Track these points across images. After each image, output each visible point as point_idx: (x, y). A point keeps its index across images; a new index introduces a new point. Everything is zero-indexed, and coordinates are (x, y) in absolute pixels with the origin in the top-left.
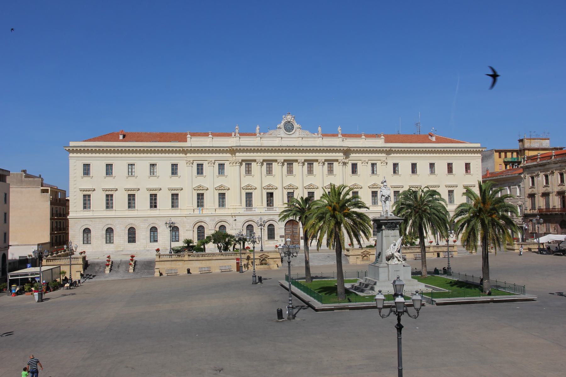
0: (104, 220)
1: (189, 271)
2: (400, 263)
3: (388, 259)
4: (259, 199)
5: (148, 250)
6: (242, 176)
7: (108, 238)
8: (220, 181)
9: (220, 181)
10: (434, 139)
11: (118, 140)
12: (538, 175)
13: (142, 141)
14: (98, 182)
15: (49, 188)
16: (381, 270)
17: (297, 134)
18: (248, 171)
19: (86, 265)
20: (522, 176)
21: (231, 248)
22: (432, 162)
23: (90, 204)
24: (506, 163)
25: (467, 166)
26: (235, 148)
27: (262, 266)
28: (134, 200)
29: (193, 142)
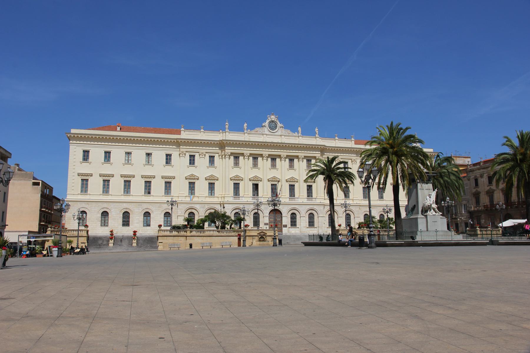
0: (100, 204)
1: (191, 246)
4: (246, 189)
8: (211, 172)
14: (96, 166)
15: (41, 182)
17: (279, 133)
21: (228, 227)
27: (261, 243)
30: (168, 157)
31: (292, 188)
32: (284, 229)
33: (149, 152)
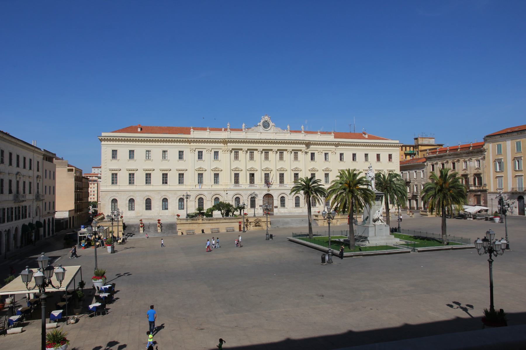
0: (127, 193)
1: (203, 231)
2: (383, 224)
3: (375, 221)
5: (161, 216)
6: (232, 161)
7: (130, 207)
8: (216, 164)
9: (216, 164)
10: (366, 136)
11: (137, 132)
12: (437, 164)
13: (156, 133)
14: (123, 164)
16: (370, 229)
17: (272, 131)
18: (236, 157)
19: (125, 227)
20: (425, 164)
21: (231, 214)
22: (366, 153)
23: (117, 180)
24: (406, 155)
25: (390, 156)
26: (227, 140)
27: (257, 228)
28: (150, 177)
29: (195, 134)
30: (181, 154)
31: (282, 176)
32: (275, 210)
33: (165, 149)
